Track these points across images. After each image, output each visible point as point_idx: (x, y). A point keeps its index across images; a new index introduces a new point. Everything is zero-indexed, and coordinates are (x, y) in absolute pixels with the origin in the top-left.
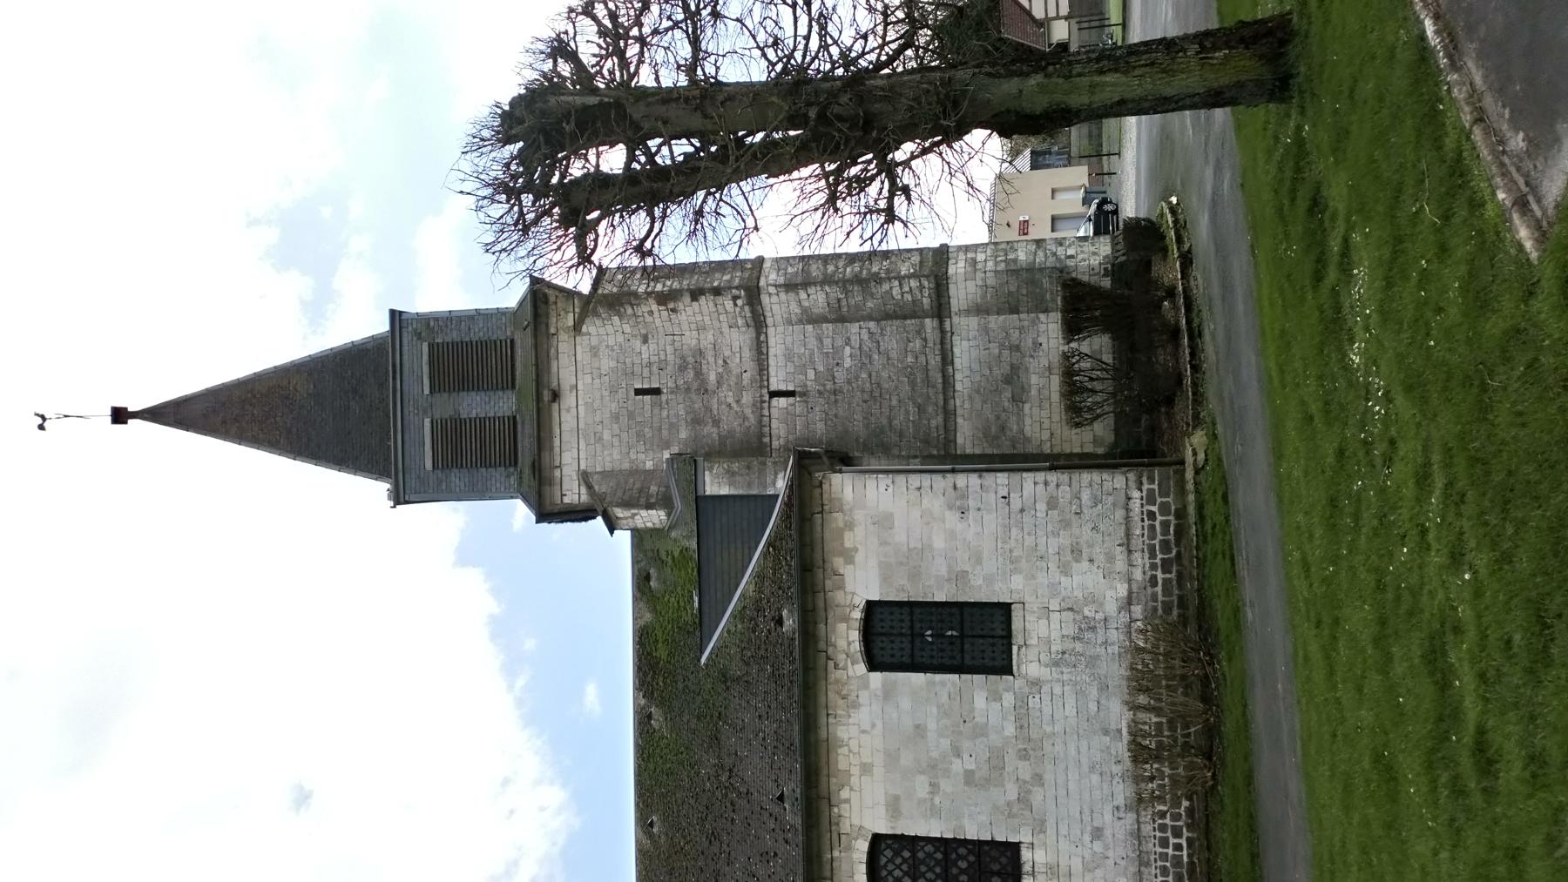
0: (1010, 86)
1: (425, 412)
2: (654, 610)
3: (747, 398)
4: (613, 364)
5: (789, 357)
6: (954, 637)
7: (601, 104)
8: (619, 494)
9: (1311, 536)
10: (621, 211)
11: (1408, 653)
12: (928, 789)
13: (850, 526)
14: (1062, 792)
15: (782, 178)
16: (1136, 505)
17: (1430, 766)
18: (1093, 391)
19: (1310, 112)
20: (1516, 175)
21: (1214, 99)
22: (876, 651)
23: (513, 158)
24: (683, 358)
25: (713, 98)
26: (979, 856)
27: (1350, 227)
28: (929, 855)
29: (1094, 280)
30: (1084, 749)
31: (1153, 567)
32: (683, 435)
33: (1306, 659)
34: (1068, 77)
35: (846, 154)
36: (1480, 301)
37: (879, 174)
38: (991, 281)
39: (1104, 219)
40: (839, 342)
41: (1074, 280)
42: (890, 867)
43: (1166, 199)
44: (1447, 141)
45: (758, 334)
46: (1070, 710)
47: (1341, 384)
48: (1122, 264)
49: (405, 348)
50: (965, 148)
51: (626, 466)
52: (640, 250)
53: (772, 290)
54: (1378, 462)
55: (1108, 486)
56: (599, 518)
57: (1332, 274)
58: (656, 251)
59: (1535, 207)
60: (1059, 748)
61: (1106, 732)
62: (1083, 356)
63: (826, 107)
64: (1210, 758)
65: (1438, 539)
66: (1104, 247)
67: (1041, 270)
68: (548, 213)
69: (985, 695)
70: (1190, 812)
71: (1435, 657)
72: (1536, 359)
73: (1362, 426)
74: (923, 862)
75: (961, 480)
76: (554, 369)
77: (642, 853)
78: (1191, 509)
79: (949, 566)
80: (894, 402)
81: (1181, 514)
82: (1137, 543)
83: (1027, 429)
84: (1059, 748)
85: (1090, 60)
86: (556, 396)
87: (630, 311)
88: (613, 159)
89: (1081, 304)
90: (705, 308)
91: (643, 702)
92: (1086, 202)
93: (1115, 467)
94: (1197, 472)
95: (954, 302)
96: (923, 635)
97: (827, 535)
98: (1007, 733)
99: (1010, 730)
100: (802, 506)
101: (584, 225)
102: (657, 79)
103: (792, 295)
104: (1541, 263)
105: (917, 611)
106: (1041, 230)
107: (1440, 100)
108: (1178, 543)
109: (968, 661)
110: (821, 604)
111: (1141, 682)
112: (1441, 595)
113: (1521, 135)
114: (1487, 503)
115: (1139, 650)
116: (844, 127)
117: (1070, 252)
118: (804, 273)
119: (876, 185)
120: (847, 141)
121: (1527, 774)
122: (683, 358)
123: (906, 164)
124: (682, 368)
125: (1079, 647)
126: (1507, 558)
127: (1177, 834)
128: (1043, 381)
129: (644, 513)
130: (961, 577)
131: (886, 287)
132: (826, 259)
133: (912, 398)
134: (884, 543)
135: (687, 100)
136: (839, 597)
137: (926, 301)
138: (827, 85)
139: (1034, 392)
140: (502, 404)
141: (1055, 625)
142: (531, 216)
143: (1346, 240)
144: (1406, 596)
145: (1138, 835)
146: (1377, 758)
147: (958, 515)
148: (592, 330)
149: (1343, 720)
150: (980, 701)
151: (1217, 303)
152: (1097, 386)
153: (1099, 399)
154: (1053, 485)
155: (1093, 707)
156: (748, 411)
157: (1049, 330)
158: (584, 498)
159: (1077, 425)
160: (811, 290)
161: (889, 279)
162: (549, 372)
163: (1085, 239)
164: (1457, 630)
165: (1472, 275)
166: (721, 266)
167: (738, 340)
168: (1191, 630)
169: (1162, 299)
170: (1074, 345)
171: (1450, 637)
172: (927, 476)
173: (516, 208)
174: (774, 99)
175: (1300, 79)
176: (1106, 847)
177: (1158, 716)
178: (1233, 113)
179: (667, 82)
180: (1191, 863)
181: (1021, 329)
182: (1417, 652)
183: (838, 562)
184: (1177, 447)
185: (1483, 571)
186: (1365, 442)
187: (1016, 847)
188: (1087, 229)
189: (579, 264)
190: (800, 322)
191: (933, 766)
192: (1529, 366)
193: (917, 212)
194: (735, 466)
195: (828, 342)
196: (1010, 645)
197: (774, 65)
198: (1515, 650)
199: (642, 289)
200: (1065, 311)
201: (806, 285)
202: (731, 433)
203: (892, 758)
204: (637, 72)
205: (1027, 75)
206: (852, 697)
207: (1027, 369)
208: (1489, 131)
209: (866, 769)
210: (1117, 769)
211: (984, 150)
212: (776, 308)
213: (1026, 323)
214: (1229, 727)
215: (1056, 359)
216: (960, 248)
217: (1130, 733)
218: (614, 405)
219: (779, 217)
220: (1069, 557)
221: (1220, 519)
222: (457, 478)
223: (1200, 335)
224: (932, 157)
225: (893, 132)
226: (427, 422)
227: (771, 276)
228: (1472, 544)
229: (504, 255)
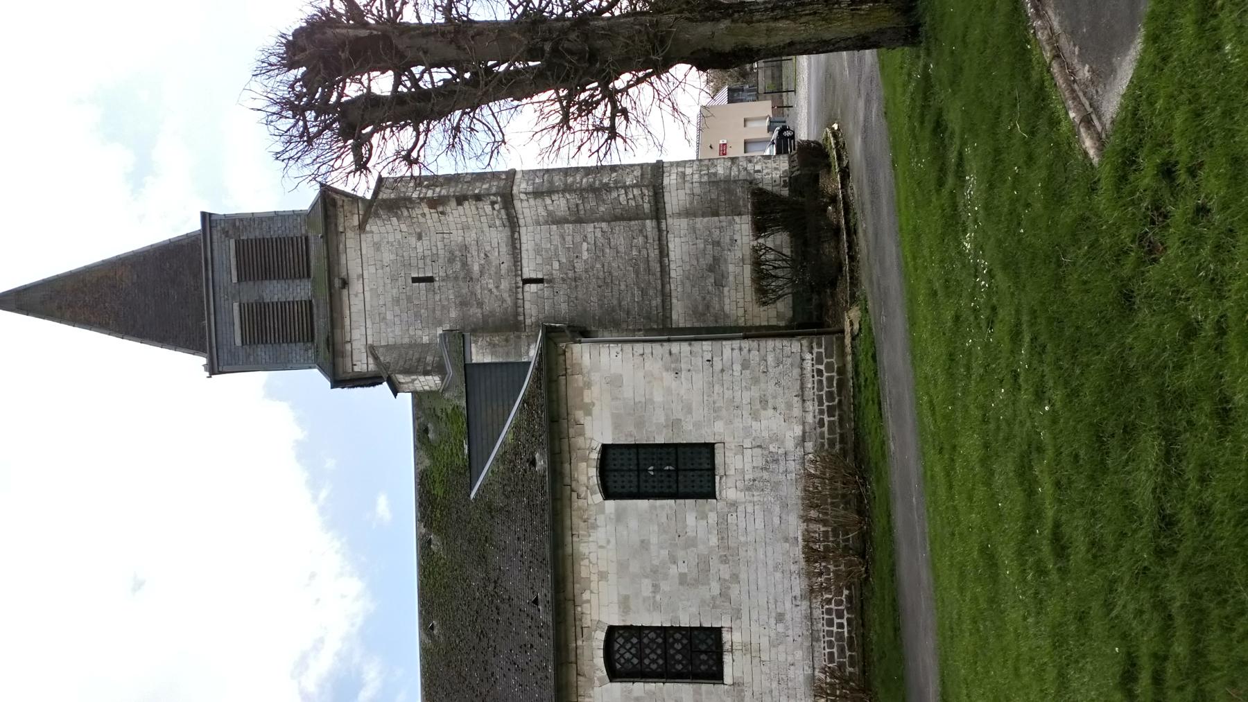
0: (706, 29)
1: (234, 298)
2: (432, 457)
3: (505, 285)
4: (393, 257)
5: (538, 251)
6: (670, 471)
7: (371, 36)
8: (401, 363)
9: (936, 385)
10: (391, 126)
11: (1005, 469)
12: (651, 589)
13: (588, 385)
14: (753, 587)
15: (524, 101)
16: (808, 365)
17: (1020, 554)
18: (777, 277)
19: (934, 54)
20: (1084, 100)
21: (861, 43)
22: (610, 484)
23: (297, 81)
24: (451, 252)
25: (464, 32)
26: (690, 639)
27: (964, 143)
28: (652, 641)
29: (776, 189)
30: (769, 554)
31: (821, 412)
32: (453, 314)
33: (933, 477)
34: (749, 23)
35: (576, 81)
36: (1056, 197)
37: (603, 99)
38: (697, 191)
39: (784, 142)
40: (578, 239)
41: (760, 189)
42: (622, 651)
43: (830, 126)
44: (1033, 73)
45: (513, 232)
46: (759, 524)
47: (958, 265)
48: (797, 178)
49: (215, 245)
50: (671, 78)
51: (406, 340)
52: (409, 160)
53: (523, 196)
54: (984, 324)
55: (787, 350)
56: (385, 384)
57: (950, 180)
58: (421, 160)
59: (1096, 122)
60: (751, 553)
61: (786, 540)
62: (768, 249)
63: (557, 43)
64: (863, 557)
65: (1026, 381)
66: (783, 164)
67: (735, 181)
68: (328, 127)
69: (694, 514)
70: (849, 598)
71: (1024, 472)
72: (1097, 240)
73: (972, 297)
74: (648, 646)
75: (675, 347)
76: (343, 261)
77: (425, 652)
78: (849, 367)
79: (667, 415)
80: (623, 287)
81: (842, 371)
82: (809, 394)
83: (727, 308)
84: (751, 553)
85: (766, 10)
86: (345, 283)
87: (406, 213)
88: (382, 84)
89: (766, 209)
90: (468, 211)
91: (424, 531)
92: (770, 129)
93: (792, 336)
94: (853, 338)
95: (668, 207)
96: (647, 470)
97: (570, 392)
98: (711, 544)
99: (714, 541)
100: (550, 370)
101: (359, 137)
102: (418, 17)
103: (539, 201)
104: (1100, 165)
105: (642, 451)
106: (736, 151)
107: (1028, 42)
108: (839, 394)
109: (681, 489)
110: (566, 448)
111: (811, 500)
112: (1028, 424)
113: (1087, 67)
114: (1060, 352)
115: (810, 475)
116: (574, 59)
117: (758, 167)
118: (548, 184)
119: (601, 107)
120: (576, 71)
121: (1090, 556)
122: (451, 252)
123: (625, 91)
124: (451, 260)
125: (766, 475)
126: (1074, 393)
127: (840, 615)
128: (738, 270)
129: (422, 378)
130: (675, 424)
131: (614, 194)
132: (566, 172)
133: (637, 284)
134: (615, 398)
135: (443, 34)
136: (580, 442)
137: (646, 206)
138: (560, 24)
139: (731, 278)
140: (300, 291)
141: (748, 458)
142: (313, 130)
143: (960, 154)
144: (1004, 426)
145: (811, 618)
146: (983, 550)
147: (673, 375)
148: (374, 228)
149: (959, 523)
150: (691, 519)
151: (868, 206)
152: (780, 273)
153: (780, 283)
154: (745, 351)
155: (776, 521)
156: (506, 295)
157: (743, 227)
158: (372, 367)
159: (764, 304)
160: (555, 197)
161: (617, 188)
162: (339, 264)
163: (769, 157)
164: (1040, 449)
165: (1051, 178)
166: (480, 177)
167: (497, 237)
168: (849, 460)
169: (827, 205)
170: (761, 241)
171: (1035, 455)
172: (649, 345)
173: (301, 123)
174: (516, 35)
175: (926, 27)
176: (787, 628)
177: (824, 525)
178: (879, 56)
179: (426, 20)
180: (850, 638)
181: (721, 228)
182: (1011, 467)
183: (579, 415)
184: (839, 319)
185: (1058, 405)
186: (974, 309)
187: (718, 631)
188: (771, 150)
189: (356, 170)
190: (546, 223)
191: (655, 571)
192: (1091, 246)
193: (634, 130)
194: (496, 339)
195: (569, 239)
196: (714, 476)
197: (515, 8)
198: (1081, 462)
199: (415, 195)
200: (754, 214)
201: (550, 192)
202: (492, 313)
203: (622, 566)
204: (401, 12)
205: (718, 20)
206: (591, 521)
207: (726, 260)
208: (1064, 65)
209: (603, 576)
210: (794, 568)
211: (689, 85)
212: (527, 211)
213: (724, 224)
214: (877, 534)
215: (747, 252)
216: (672, 164)
217: (804, 540)
218: (395, 291)
219: (524, 136)
220: (759, 406)
221: (870, 374)
222: (261, 351)
223: (855, 232)
224: (644, 85)
225: (613, 64)
226: (236, 306)
227: (521, 186)
228: (1051, 383)
229: (292, 162)
